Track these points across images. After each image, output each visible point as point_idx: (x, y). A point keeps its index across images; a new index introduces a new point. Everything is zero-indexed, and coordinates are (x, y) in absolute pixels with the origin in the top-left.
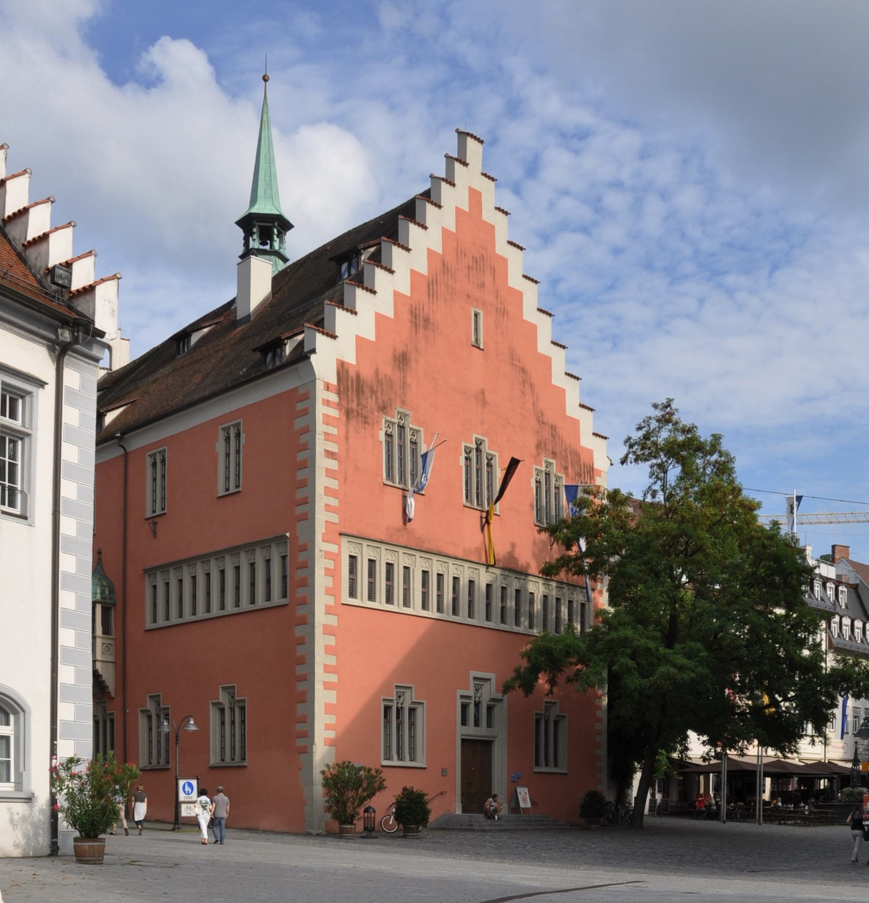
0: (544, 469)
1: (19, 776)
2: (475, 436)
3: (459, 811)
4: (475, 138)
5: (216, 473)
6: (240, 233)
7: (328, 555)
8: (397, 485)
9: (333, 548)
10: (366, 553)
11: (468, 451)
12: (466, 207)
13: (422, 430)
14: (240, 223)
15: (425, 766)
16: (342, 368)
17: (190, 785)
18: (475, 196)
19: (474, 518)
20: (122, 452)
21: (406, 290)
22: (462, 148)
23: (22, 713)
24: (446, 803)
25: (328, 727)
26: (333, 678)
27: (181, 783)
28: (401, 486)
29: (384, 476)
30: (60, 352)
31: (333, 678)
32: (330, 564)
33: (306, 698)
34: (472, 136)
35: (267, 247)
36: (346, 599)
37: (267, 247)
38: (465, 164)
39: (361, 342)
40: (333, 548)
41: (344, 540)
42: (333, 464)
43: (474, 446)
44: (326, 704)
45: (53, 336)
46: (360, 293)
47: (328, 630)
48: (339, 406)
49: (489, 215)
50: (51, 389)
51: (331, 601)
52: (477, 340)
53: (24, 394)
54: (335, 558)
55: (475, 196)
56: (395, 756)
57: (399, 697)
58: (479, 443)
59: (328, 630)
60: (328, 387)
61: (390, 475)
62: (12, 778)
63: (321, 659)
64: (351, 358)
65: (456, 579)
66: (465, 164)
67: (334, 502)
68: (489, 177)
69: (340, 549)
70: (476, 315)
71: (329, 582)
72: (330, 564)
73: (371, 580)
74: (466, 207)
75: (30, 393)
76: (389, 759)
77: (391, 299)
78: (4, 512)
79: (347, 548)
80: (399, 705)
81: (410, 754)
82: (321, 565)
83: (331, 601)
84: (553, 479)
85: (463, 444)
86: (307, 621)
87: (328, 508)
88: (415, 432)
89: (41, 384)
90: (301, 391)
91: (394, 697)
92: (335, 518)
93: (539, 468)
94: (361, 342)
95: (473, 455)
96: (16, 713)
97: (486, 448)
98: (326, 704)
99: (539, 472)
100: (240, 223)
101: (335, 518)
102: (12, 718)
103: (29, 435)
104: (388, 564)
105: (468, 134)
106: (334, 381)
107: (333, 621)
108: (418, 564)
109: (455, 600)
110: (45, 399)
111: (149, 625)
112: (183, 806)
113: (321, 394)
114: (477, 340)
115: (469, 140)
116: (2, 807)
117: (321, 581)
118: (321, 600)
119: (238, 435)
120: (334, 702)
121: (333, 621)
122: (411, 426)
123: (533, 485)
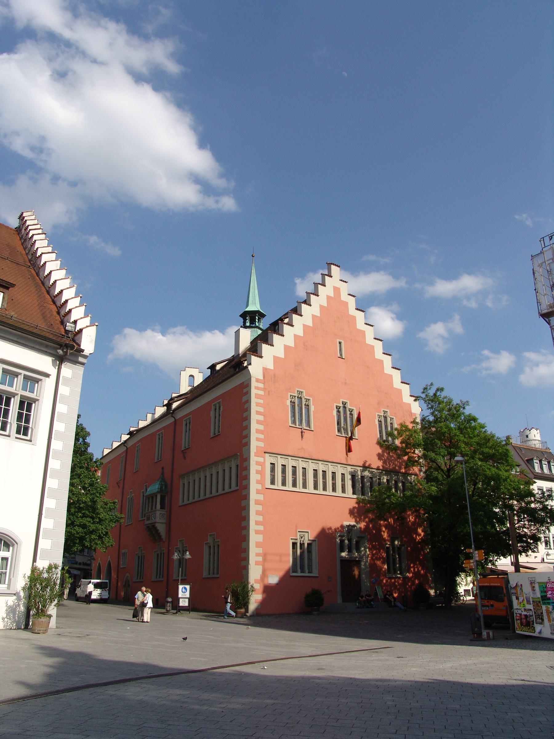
0: (382, 415)
1: (10, 580)
2: (341, 400)
3: (339, 600)
4: (335, 265)
5: (210, 426)
6: (241, 320)
7: (258, 463)
8: (298, 426)
9: (261, 460)
10: (280, 462)
11: (338, 408)
12: (332, 295)
13: (311, 399)
14: (241, 316)
15: (318, 575)
16: (265, 370)
17: (186, 588)
18: (337, 290)
19: (342, 442)
20: (173, 420)
21: (301, 334)
22: (329, 270)
23: (16, 545)
24: (335, 597)
25: (257, 555)
26: (261, 528)
27: (181, 587)
28: (300, 427)
29: (290, 422)
30: (60, 360)
31: (261, 528)
32: (259, 468)
33: (245, 539)
34: (334, 264)
35: (254, 325)
36: (269, 485)
37: (254, 325)
38: (331, 277)
39: (276, 359)
40: (261, 460)
41: (267, 455)
42: (261, 418)
43: (341, 405)
44: (256, 542)
45: (55, 353)
46: (275, 336)
47: (257, 502)
48: (264, 389)
49: (344, 297)
50: (53, 378)
51: (259, 487)
52: (341, 355)
53: (37, 381)
54: (262, 464)
55: (337, 290)
56: (299, 570)
57: (302, 537)
58: (344, 404)
59: (257, 502)
60: (258, 380)
61: (294, 422)
62: (7, 582)
63: (254, 517)
64: (271, 366)
65: (334, 473)
66: (331, 277)
67: (261, 436)
68: (344, 281)
69: (265, 460)
70: (340, 343)
71: (259, 477)
72: (259, 468)
73: (334, 482)
74: (332, 295)
75: (41, 380)
76: (296, 572)
77: (293, 338)
78: (16, 438)
79: (269, 459)
80: (302, 542)
81: (308, 569)
82: (254, 468)
83: (259, 487)
84: (389, 419)
85: (335, 404)
86: (246, 497)
87: (258, 439)
88: (307, 400)
89: (47, 375)
90: (245, 384)
91: (298, 537)
92: (262, 444)
93: (380, 414)
94: (276, 359)
95: (341, 410)
96: (13, 545)
97: (348, 406)
98: (256, 542)
99: (380, 416)
100: (241, 316)
101: (262, 444)
102: (11, 548)
103: (38, 400)
104: (323, 471)
105: (332, 264)
106: (261, 377)
107: (261, 497)
108: (311, 467)
109: (363, 487)
110: (48, 384)
111: (181, 504)
112: (181, 600)
113: (254, 384)
114: (341, 355)
115: (332, 266)
116: (3, 599)
117: (254, 477)
118: (254, 486)
119: (220, 407)
120: (262, 541)
121: (261, 497)
122: (306, 397)
123: (377, 423)
